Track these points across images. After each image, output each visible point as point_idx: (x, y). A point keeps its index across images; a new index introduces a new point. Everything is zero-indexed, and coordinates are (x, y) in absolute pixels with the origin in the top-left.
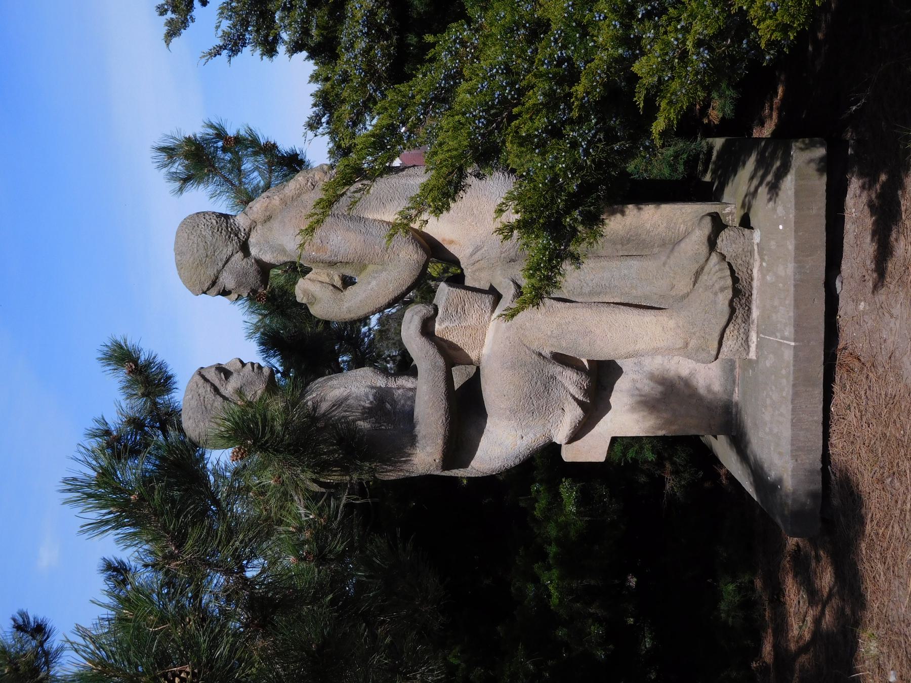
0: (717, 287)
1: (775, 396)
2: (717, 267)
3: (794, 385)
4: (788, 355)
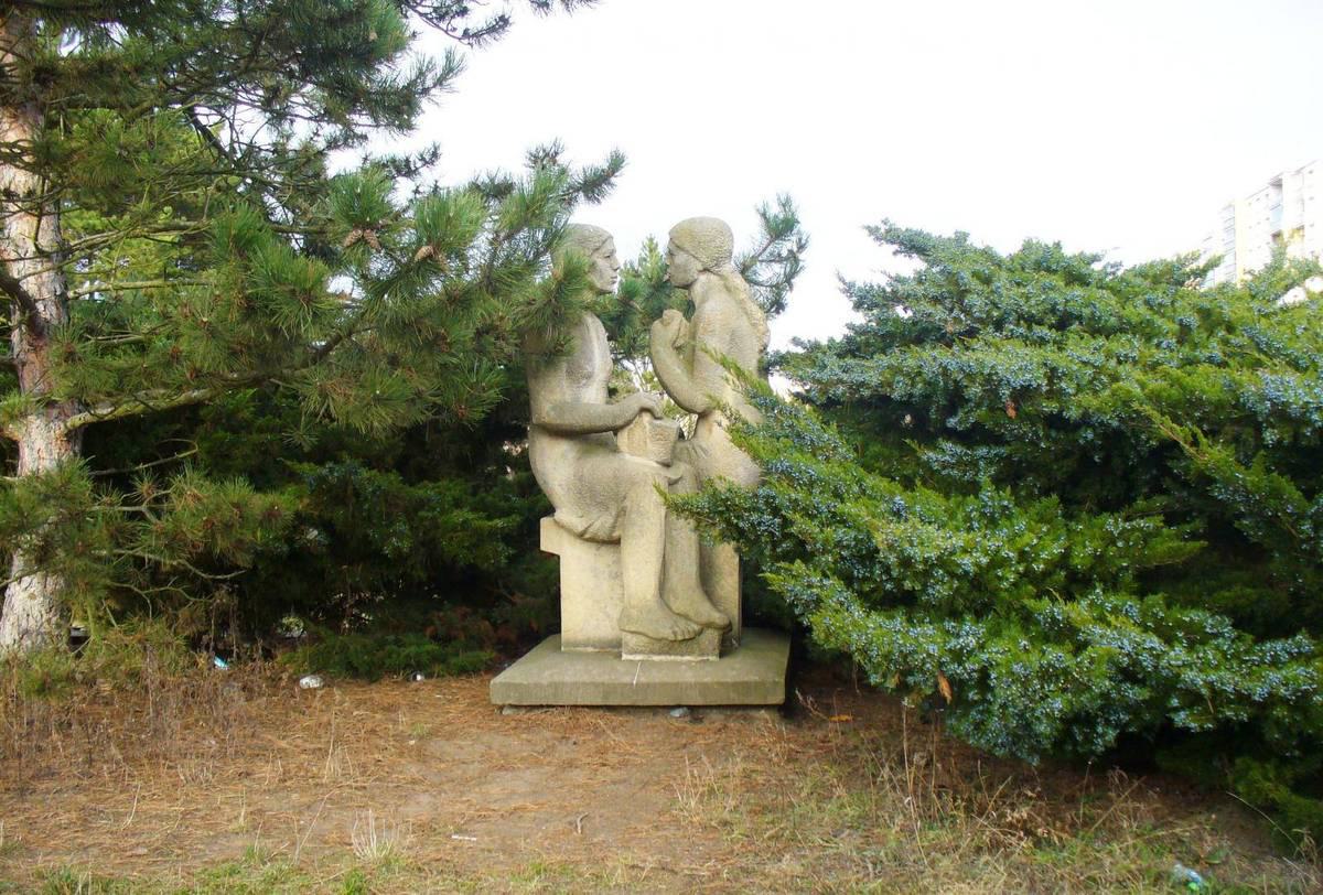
0: (677, 629)
1: (594, 672)
2: (691, 630)
3: (603, 684)
4: (626, 679)
